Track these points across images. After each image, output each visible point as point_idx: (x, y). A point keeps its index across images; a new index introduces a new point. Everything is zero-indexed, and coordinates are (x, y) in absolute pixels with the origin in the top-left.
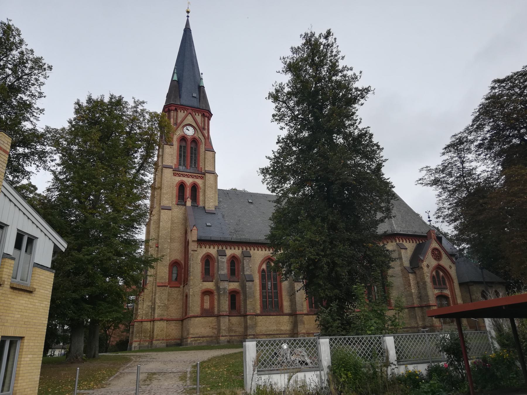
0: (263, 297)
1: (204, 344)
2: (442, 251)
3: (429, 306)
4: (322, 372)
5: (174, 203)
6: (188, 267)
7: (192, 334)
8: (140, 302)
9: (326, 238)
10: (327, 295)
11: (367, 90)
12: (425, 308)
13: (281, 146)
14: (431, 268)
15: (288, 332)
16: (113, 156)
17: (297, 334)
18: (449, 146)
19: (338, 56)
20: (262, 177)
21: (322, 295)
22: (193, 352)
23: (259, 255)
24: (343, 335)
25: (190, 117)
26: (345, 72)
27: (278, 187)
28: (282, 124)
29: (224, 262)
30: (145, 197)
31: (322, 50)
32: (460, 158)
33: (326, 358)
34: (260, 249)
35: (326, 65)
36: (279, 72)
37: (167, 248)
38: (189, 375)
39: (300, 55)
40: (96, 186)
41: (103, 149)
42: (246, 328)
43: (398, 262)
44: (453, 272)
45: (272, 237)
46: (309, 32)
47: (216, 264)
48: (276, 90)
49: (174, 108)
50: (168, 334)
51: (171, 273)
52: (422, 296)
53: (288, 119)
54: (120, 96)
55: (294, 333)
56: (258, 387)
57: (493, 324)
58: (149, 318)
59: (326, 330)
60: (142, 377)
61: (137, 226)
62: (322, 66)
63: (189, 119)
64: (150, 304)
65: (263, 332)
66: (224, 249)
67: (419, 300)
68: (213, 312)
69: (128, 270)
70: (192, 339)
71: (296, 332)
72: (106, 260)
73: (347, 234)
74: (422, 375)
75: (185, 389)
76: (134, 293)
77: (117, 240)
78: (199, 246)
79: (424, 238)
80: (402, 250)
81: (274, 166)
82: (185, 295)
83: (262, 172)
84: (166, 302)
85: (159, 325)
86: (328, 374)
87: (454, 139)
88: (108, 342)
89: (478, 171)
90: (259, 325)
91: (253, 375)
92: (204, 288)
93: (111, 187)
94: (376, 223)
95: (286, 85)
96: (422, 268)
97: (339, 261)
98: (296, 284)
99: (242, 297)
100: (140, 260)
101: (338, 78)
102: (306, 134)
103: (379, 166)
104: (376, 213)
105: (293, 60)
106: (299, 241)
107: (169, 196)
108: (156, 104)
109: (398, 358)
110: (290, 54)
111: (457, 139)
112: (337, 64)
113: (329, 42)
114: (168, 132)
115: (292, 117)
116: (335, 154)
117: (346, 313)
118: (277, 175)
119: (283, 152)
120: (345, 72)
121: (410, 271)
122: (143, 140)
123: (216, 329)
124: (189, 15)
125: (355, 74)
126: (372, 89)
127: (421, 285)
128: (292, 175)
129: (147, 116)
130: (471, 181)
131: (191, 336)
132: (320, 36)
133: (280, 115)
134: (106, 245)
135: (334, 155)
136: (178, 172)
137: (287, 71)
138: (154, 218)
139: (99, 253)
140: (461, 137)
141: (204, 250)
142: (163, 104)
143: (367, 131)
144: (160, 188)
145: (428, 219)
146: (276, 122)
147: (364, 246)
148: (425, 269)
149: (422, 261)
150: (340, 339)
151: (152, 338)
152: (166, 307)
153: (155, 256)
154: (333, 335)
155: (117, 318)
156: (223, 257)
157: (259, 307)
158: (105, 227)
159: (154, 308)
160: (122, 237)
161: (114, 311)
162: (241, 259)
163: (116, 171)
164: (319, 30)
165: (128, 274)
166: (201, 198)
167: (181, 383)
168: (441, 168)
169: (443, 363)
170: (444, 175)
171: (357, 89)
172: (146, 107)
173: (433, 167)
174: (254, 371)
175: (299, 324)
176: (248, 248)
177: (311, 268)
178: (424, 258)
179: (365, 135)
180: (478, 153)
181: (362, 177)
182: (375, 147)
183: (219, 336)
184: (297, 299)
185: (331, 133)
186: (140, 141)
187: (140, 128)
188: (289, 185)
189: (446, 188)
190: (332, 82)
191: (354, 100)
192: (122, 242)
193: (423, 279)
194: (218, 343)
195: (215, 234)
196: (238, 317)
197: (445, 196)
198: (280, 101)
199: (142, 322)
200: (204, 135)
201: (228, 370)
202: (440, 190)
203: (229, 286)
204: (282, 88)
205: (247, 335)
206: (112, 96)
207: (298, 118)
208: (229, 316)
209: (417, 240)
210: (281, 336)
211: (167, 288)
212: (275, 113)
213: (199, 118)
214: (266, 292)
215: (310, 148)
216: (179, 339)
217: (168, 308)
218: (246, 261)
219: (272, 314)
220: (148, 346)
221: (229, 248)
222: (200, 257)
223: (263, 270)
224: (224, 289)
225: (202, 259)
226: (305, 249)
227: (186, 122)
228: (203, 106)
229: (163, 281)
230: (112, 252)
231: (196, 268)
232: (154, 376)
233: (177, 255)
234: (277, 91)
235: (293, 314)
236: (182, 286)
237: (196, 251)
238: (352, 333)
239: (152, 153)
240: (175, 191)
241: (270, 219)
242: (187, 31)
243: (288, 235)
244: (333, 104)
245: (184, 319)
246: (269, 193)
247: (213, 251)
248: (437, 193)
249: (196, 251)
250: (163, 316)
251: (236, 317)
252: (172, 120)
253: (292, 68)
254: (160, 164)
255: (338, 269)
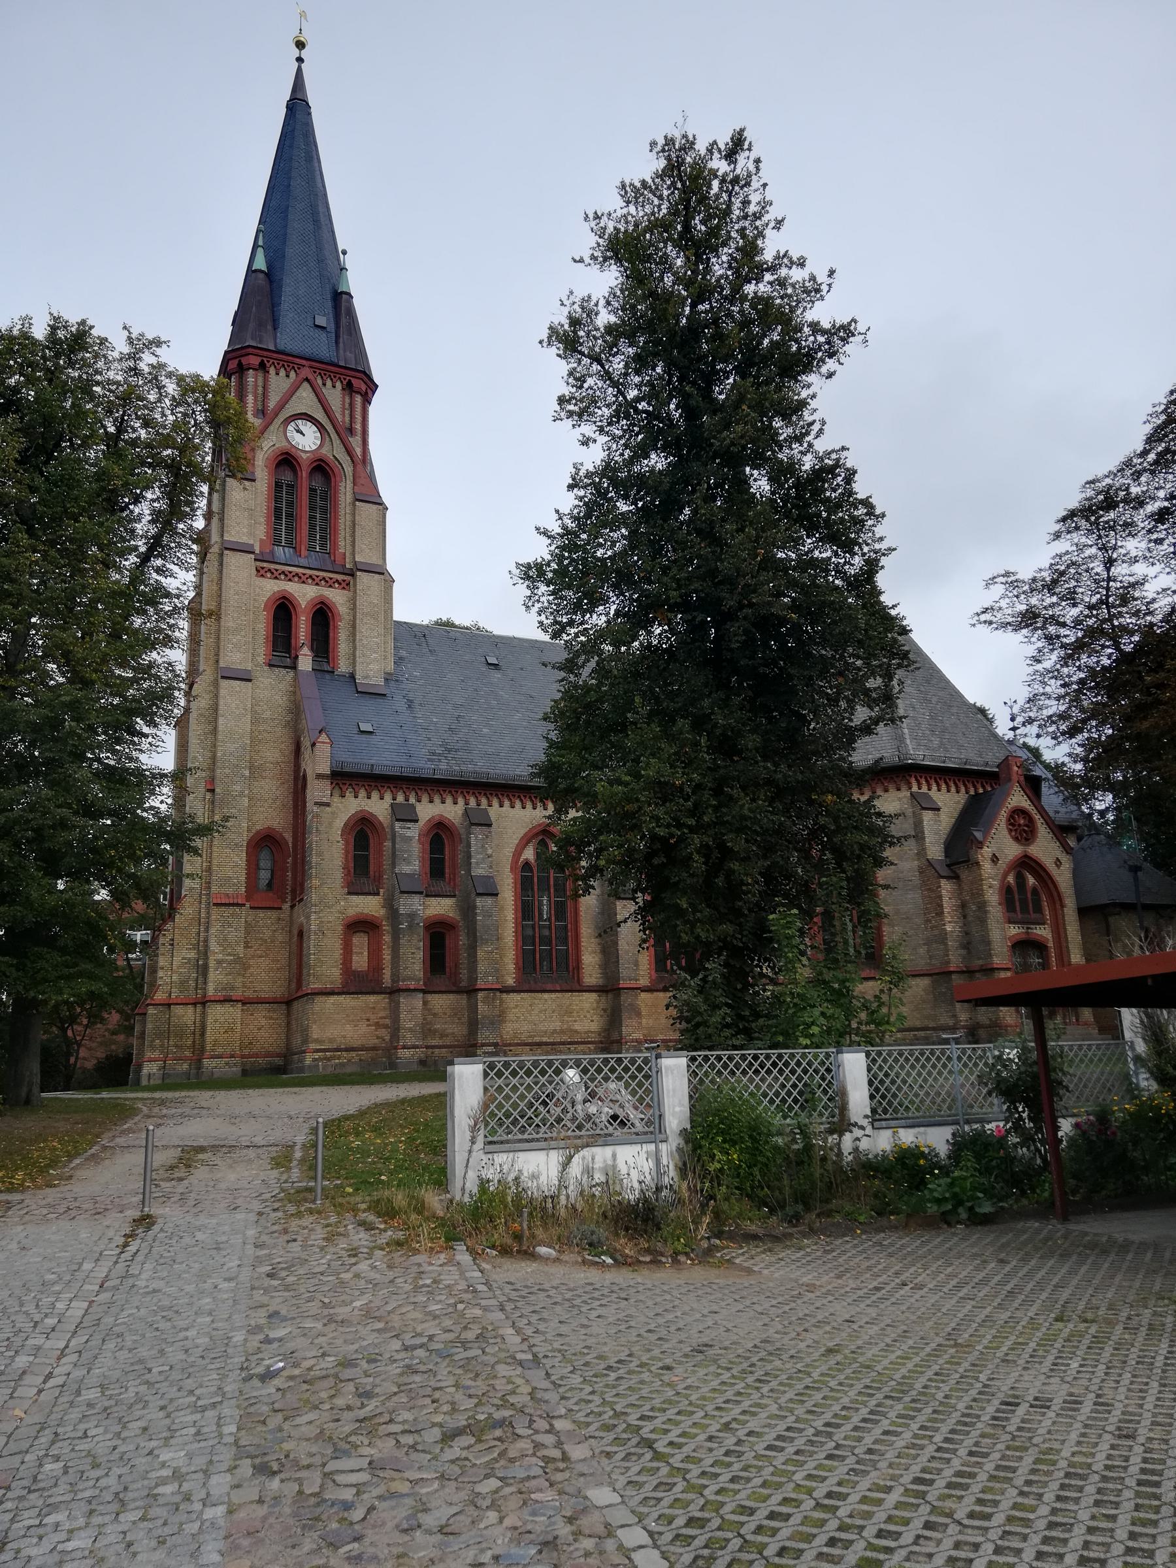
0: (525, 939)
1: (349, 1070)
2: (1037, 817)
3: (990, 970)
4: (663, 1147)
5: (261, 659)
6: (304, 852)
7: (317, 1041)
8: (162, 950)
9: (704, 776)
10: (698, 937)
11: (846, 331)
12: (978, 975)
13: (581, 499)
14: (1003, 864)
15: (593, 1037)
16: (66, 511)
17: (619, 1042)
18: (1072, 514)
19: (765, 218)
20: (523, 590)
21: (685, 938)
22: (317, 1089)
23: (515, 821)
24: (735, 1048)
25: (305, 392)
26: (783, 272)
27: (571, 623)
28: (588, 429)
29: (410, 839)
30: (168, 642)
31: (718, 196)
32: (1104, 548)
33: (677, 1109)
34: (518, 804)
35: (724, 244)
36: (581, 261)
37: (241, 794)
38: (298, 1154)
39: (648, 209)
40: (15, 606)
41: (33, 490)
42: (473, 1025)
43: (911, 846)
44: (1063, 877)
45: (549, 770)
46: (677, 135)
47: (388, 844)
48: (570, 317)
49: (255, 361)
50: (246, 1041)
51: (253, 868)
52: (973, 940)
53: (606, 412)
54: (83, 322)
55: (610, 1040)
56: (483, 1183)
57: (1142, 1022)
58: (192, 995)
59: (694, 1036)
60: (160, 1158)
61: (146, 730)
62: (715, 250)
63: (305, 399)
64: (192, 955)
65: (524, 1038)
66: (412, 800)
67: (963, 952)
68: (379, 981)
69: (121, 859)
70: (316, 1056)
71: (615, 1036)
72: (53, 827)
73: (766, 768)
74: (937, 1155)
75: (283, 1190)
76: (140, 922)
77: (82, 773)
78: (337, 792)
79: (988, 780)
80: (925, 813)
81: (560, 558)
82: (295, 932)
83: (527, 577)
84: (240, 950)
85: (218, 1015)
86: (679, 1149)
87: (1090, 493)
88: (72, 1060)
89: (1149, 591)
90: (510, 1016)
91: (470, 1152)
92: (351, 912)
93: (63, 610)
94: (849, 737)
95: (602, 302)
96: (977, 863)
97: (736, 843)
98: (619, 905)
99: (463, 940)
100: (159, 830)
101: (763, 288)
102: (657, 461)
103: (872, 566)
104: (853, 708)
105: (627, 222)
106: (626, 784)
107: (244, 639)
108: (197, 346)
109: (874, 1111)
110: (614, 204)
111: (1099, 493)
112: (759, 242)
113: (738, 171)
114: (239, 440)
115: (620, 405)
116: (741, 530)
117: (753, 986)
118: (569, 587)
119: (588, 515)
120: (783, 272)
121: (944, 871)
122: (158, 463)
123: (386, 1027)
124: (304, 54)
125: (813, 278)
126: (861, 328)
127: (972, 911)
128: (615, 586)
129: (171, 388)
130: (1128, 620)
131: (312, 1046)
132: (710, 151)
133: (581, 401)
134: (52, 785)
135: (737, 531)
136: (272, 566)
137: (605, 259)
138: (202, 704)
139: (31, 808)
140: (1110, 486)
141: (351, 805)
142: (224, 346)
143: (838, 460)
144: (216, 614)
145: (1011, 725)
146: (569, 423)
147: (811, 802)
148: (987, 867)
149: (980, 845)
150: (730, 1058)
151: (199, 1051)
152: (241, 965)
153: (202, 818)
154: (710, 1049)
155: (92, 995)
156: (409, 825)
157: (511, 967)
158: (45, 730)
159: (205, 968)
160: (99, 760)
161: (81, 975)
162: (462, 831)
163: (76, 557)
164: (709, 132)
165: (120, 870)
166: (342, 647)
167: (275, 1173)
168: (1047, 576)
169: (992, 1126)
170: (1054, 599)
171: (815, 327)
172: (165, 355)
173: (1025, 574)
174: (473, 1143)
175: (625, 1015)
176: (484, 801)
177: (656, 861)
178: (985, 837)
179: (832, 470)
180: (1155, 536)
181: (817, 603)
182: (861, 511)
183: (396, 1048)
184: (623, 945)
185: (734, 460)
186: (150, 465)
187: (147, 424)
188: (604, 618)
189: (1058, 637)
190: (744, 298)
191: (805, 362)
192: (97, 774)
193: (978, 893)
194: (392, 1065)
195: (383, 756)
196: (451, 996)
197: (1051, 660)
198: (582, 354)
199: (169, 1005)
200: (349, 452)
201: (411, 1140)
202: (1040, 644)
203: (425, 907)
204: (591, 313)
205: (475, 1046)
206: (56, 319)
207: (636, 410)
208: (424, 992)
209: (970, 786)
210: (572, 1047)
211: (244, 911)
212: (566, 391)
213: (335, 395)
214: (533, 927)
215: (671, 506)
216: (278, 1055)
217: (246, 967)
218: (476, 837)
219: (549, 987)
220: (187, 1075)
221: (425, 798)
222: (340, 823)
223: (527, 864)
224: (412, 916)
225: (348, 828)
226: (640, 808)
227: (293, 408)
228: (346, 358)
229: (230, 891)
230: (69, 806)
231: (329, 853)
232: (200, 1156)
233: (271, 815)
234: (575, 322)
235: (610, 988)
236: (286, 906)
237: (328, 805)
238: (759, 1043)
239: (190, 504)
240: (262, 625)
241: (545, 719)
242: (298, 109)
243: (597, 768)
244: (742, 371)
245: (293, 998)
246: (546, 638)
247: (379, 806)
248: (1031, 650)
249: (328, 805)
250: (233, 988)
251: (444, 996)
252: (250, 399)
253: (623, 248)
254: (215, 538)
255: (735, 866)
